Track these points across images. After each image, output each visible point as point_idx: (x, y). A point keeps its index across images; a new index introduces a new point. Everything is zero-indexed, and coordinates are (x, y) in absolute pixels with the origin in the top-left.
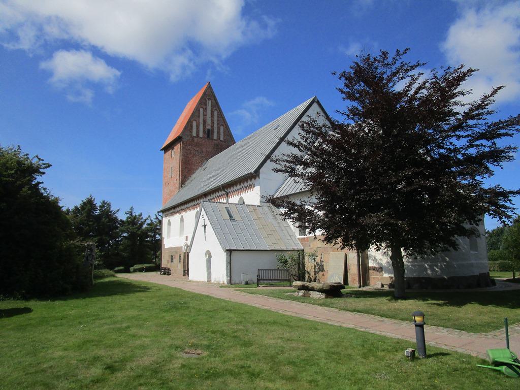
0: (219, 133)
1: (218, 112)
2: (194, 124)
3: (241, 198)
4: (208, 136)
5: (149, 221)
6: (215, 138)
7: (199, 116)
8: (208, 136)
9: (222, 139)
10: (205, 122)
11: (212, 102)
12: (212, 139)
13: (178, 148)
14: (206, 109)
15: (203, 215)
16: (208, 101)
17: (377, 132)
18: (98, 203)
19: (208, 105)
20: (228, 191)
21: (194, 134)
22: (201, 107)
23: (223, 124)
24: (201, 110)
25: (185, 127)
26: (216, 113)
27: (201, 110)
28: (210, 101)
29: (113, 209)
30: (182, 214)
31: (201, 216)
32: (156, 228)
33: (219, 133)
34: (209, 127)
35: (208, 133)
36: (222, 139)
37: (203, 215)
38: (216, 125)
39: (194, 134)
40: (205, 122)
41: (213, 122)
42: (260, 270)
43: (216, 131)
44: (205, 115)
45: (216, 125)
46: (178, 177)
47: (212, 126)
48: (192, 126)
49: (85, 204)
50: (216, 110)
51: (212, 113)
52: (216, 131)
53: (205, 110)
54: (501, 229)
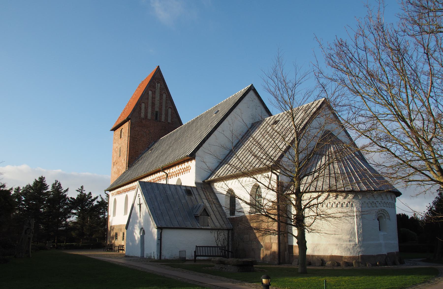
0: (167, 115)
1: (166, 96)
2: (143, 105)
3: (179, 180)
4: (156, 118)
5: (99, 199)
6: (163, 119)
7: (148, 99)
8: (156, 118)
9: (169, 121)
10: (153, 104)
11: (161, 85)
12: (160, 121)
13: (127, 125)
14: (155, 92)
15: (139, 195)
16: (157, 84)
17: (88, 207)
18: (49, 183)
19: (156, 88)
20: (168, 173)
21: (143, 115)
22: (150, 90)
23: (171, 106)
24: (150, 92)
25: (134, 108)
26: (164, 96)
27: (150, 92)
28: (159, 85)
29: (64, 188)
30: (127, 193)
31: (137, 196)
32: (104, 205)
33: (167, 115)
34: (157, 109)
35: (156, 116)
36: (169, 121)
37: (139, 195)
38: (164, 108)
39: (143, 115)
40: (153, 104)
41: (161, 104)
42: (198, 247)
43: (163, 113)
44: (153, 98)
45: (164, 108)
46: (126, 157)
47: (161, 109)
48: (140, 108)
49: (36, 183)
50: (165, 93)
51: (161, 95)
52: (163, 113)
53: (154, 93)
54: (80, 195)
